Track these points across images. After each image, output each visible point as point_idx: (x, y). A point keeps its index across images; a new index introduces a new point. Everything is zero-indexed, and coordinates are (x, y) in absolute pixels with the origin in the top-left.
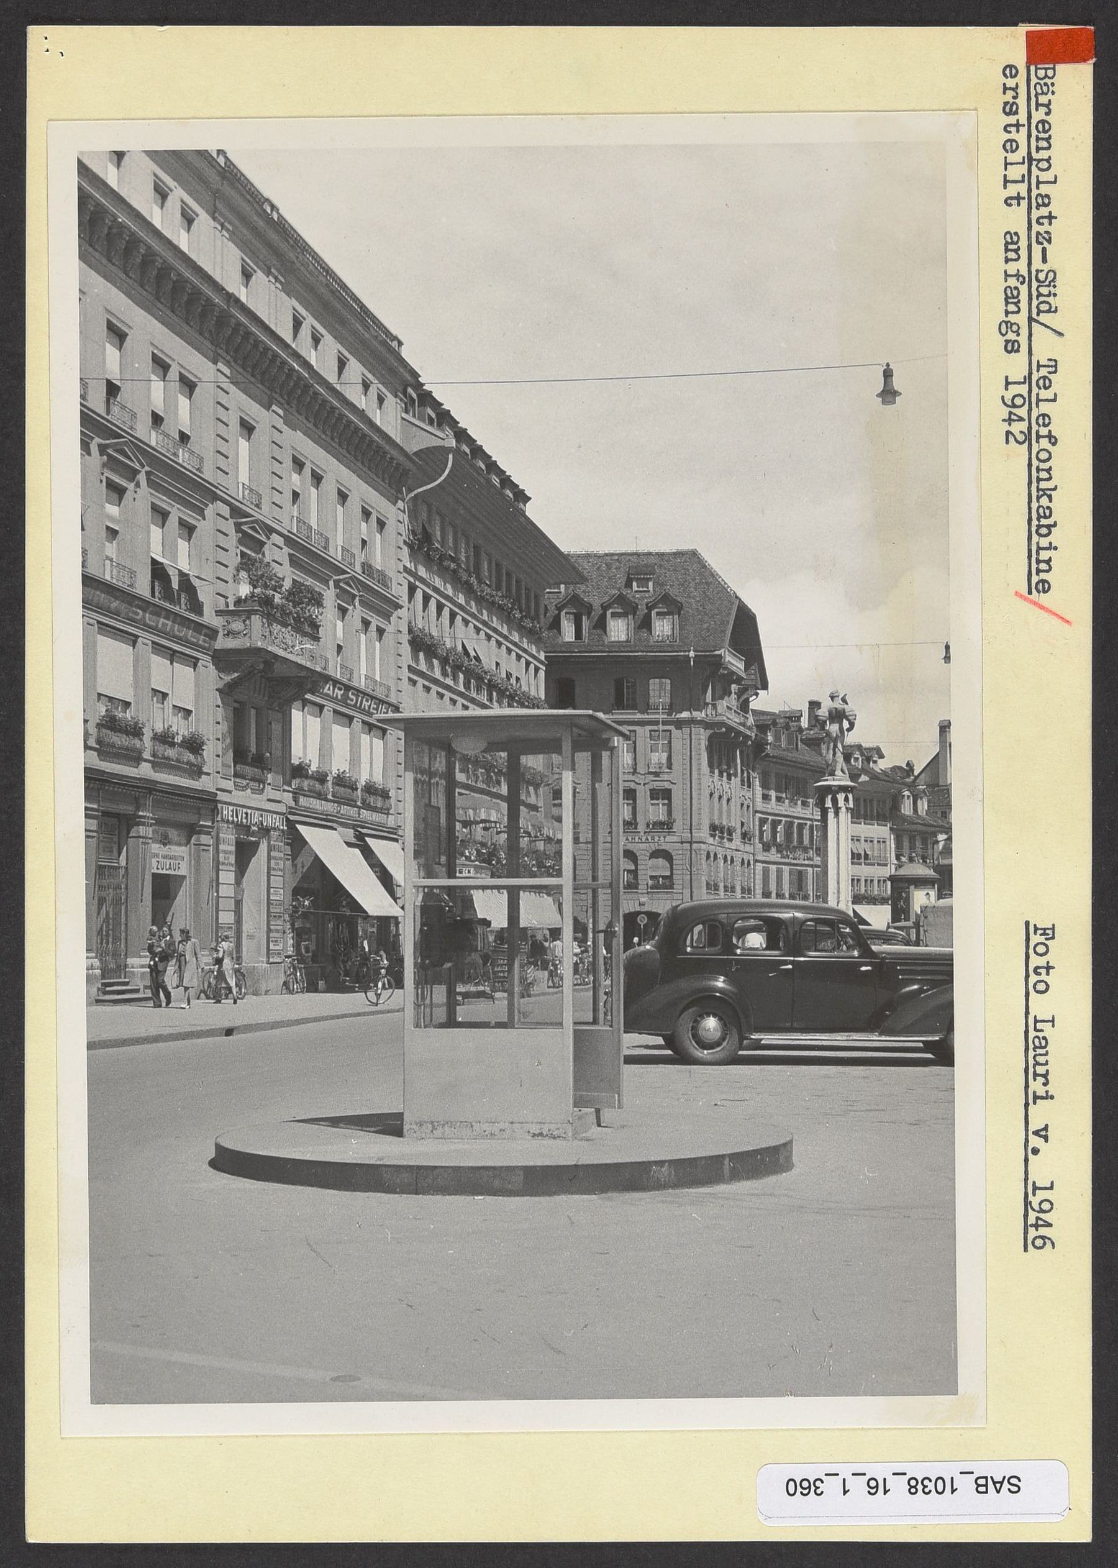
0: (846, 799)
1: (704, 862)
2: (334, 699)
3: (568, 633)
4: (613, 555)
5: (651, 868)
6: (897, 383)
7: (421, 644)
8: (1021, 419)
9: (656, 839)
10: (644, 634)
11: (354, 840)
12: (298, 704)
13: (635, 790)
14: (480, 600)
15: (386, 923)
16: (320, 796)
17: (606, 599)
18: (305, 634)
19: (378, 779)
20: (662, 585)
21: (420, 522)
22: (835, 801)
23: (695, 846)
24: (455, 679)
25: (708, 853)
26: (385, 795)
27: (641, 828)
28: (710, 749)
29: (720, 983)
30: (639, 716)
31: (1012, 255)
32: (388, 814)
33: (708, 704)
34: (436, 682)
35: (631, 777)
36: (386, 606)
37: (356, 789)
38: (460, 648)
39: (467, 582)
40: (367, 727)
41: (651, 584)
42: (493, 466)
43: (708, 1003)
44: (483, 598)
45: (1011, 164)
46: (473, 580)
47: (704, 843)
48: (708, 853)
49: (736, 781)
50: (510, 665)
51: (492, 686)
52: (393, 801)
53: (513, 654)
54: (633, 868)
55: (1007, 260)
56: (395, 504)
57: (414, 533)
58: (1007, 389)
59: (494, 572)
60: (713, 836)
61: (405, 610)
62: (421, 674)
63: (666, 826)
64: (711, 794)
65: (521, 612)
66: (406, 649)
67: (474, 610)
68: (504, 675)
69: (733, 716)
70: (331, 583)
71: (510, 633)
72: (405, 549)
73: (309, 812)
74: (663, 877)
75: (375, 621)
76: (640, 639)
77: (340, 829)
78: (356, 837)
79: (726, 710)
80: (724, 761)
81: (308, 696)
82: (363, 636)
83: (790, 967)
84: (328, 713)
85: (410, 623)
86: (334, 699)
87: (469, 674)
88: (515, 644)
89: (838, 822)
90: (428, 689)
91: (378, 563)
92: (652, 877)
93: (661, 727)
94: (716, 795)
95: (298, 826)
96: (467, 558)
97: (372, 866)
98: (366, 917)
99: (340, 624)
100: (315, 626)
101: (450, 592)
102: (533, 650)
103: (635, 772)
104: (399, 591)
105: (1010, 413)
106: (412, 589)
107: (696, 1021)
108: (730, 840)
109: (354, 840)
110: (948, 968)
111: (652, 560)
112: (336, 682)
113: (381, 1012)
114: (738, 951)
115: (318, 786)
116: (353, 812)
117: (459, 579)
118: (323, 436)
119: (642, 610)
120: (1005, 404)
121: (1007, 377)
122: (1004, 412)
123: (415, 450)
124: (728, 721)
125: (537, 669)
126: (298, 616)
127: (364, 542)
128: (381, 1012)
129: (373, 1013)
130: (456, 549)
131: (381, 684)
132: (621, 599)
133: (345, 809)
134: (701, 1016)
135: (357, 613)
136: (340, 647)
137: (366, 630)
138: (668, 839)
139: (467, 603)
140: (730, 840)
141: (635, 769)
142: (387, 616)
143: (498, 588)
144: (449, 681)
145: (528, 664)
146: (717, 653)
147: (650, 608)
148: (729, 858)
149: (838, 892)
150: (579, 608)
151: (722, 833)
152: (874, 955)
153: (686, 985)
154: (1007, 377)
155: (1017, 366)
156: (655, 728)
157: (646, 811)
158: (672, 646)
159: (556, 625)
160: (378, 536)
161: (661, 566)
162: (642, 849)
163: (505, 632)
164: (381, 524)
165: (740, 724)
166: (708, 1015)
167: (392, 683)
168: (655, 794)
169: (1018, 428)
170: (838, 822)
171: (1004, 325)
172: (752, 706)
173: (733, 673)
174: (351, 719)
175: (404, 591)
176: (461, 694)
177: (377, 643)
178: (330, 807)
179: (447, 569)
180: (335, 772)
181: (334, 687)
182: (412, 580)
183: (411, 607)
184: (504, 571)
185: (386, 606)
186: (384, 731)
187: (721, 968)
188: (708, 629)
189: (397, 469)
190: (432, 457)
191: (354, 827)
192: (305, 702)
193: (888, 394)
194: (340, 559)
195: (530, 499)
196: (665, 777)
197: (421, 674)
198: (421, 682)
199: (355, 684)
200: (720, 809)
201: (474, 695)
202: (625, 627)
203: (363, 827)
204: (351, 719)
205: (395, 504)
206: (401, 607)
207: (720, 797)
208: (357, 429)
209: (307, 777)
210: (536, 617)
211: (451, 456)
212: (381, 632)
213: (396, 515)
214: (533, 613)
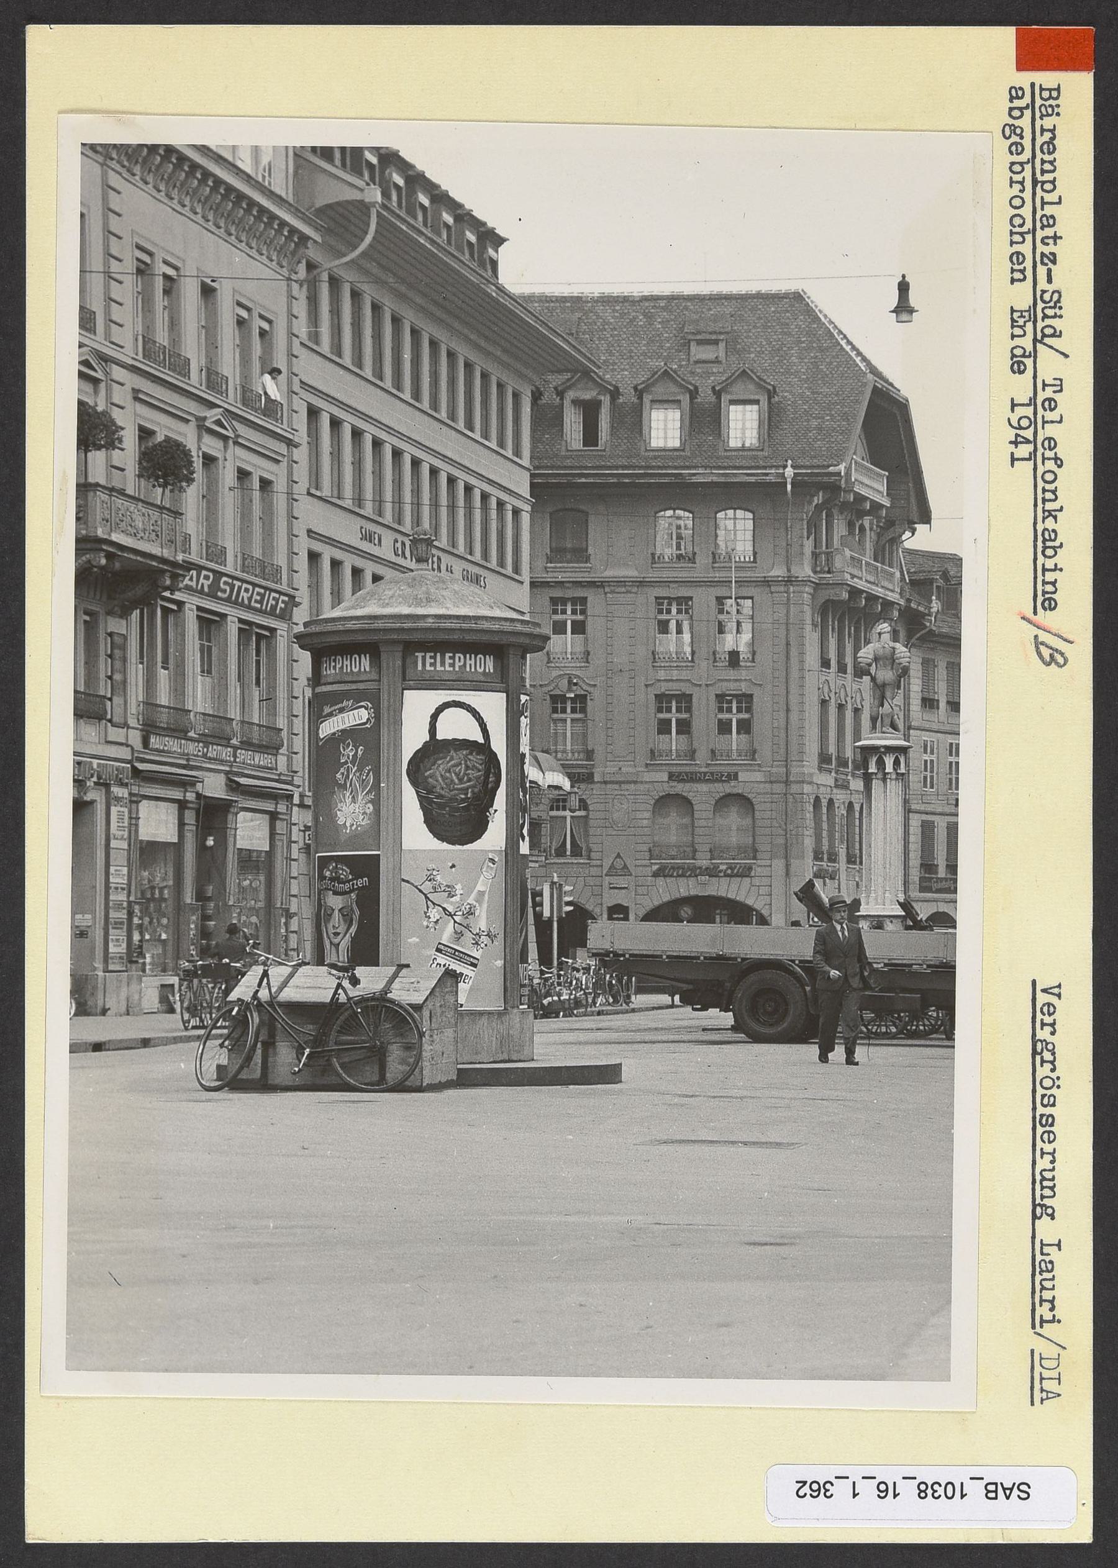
6: (913, 300)
22: (881, 764)
25: (817, 800)
31: (1018, 275)
42: (441, 198)
45: (1018, 459)
48: (817, 800)
55: (1013, 336)
58: (1013, 411)
105: (1017, 435)
116: (226, 753)
120: (1010, 424)
121: (1012, 399)
122: (1011, 434)
154: (1012, 399)
155: (1021, 386)
171: (1007, 128)
193: (903, 308)
207: (841, 707)
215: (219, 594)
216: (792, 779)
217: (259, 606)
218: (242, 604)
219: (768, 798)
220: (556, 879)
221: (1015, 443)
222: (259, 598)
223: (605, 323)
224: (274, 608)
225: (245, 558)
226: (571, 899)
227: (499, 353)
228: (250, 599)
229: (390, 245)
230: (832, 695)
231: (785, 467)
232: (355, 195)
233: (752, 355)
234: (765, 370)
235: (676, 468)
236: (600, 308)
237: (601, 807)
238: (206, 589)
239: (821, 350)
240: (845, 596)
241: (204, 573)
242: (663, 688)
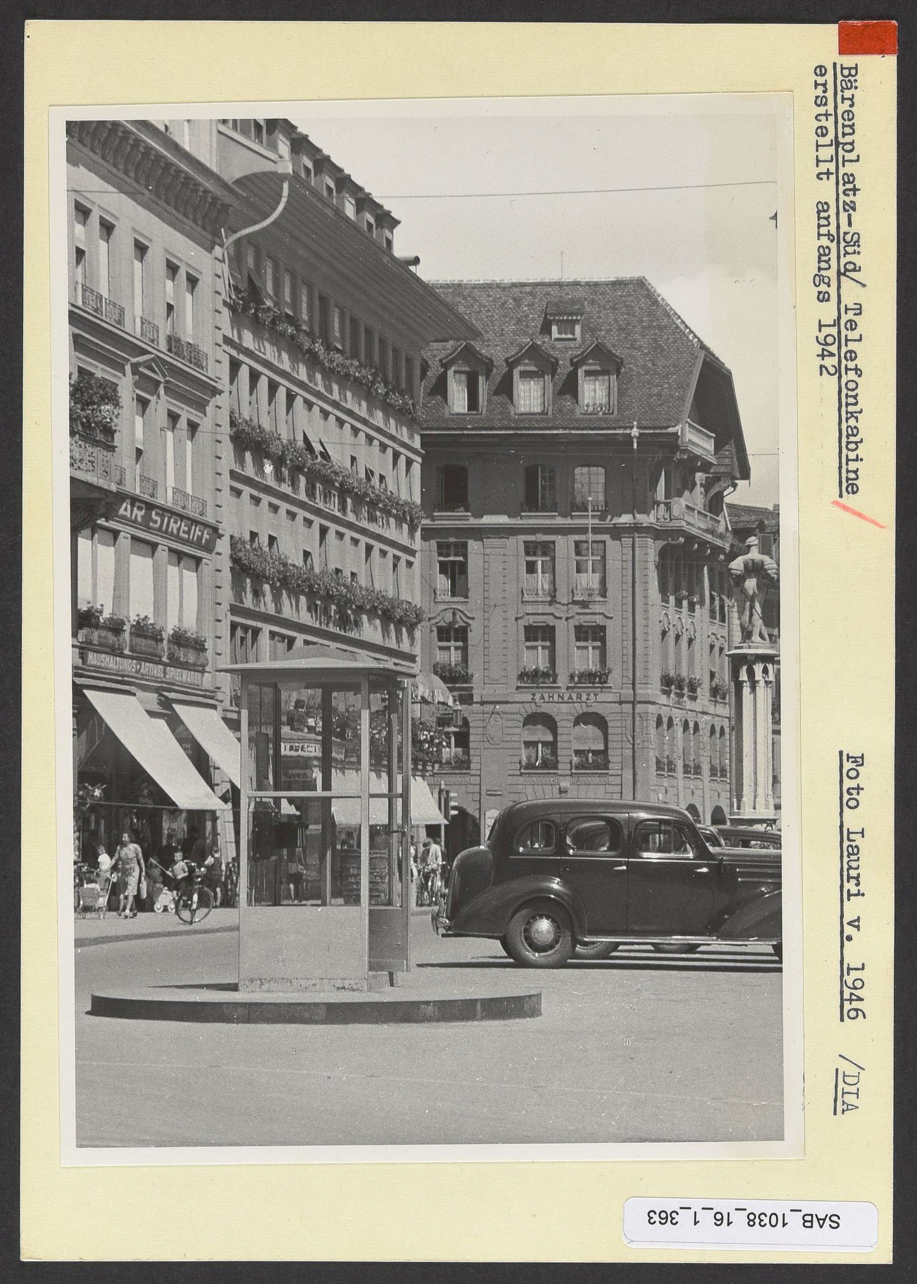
0: (765, 671)
1: (653, 731)
2: (133, 522)
3: (458, 399)
4: (523, 285)
5: (577, 739)
7: (248, 441)
8: (833, 355)
9: (584, 697)
10: (568, 403)
11: (157, 708)
12: (87, 532)
13: (554, 627)
14: (329, 374)
15: (198, 819)
16: (115, 651)
17: (513, 351)
18: (96, 443)
19: (190, 625)
20: (593, 331)
21: (245, 272)
22: (751, 673)
23: (638, 706)
24: (294, 484)
26: (199, 646)
27: (563, 680)
28: (661, 568)
29: (555, 884)
30: (559, 521)
32: (203, 672)
33: (658, 503)
34: (267, 490)
35: (548, 609)
36: (198, 393)
37: (162, 640)
38: (300, 443)
39: (309, 351)
40: (175, 556)
41: (578, 328)
43: (541, 904)
44: (332, 370)
45: (824, 326)
46: (318, 347)
47: (653, 703)
49: (702, 612)
50: (374, 460)
51: (345, 491)
52: (209, 654)
53: (376, 442)
54: (550, 738)
56: (210, 250)
57: (237, 289)
58: (820, 331)
59: (348, 331)
60: (667, 693)
61: (226, 394)
62: (248, 481)
63: (596, 679)
64: (664, 633)
65: (386, 385)
66: (227, 449)
67: (320, 388)
68: (362, 475)
69: (695, 520)
70: (128, 368)
71: (371, 414)
72: (226, 312)
73: (100, 672)
74: (595, 753)
75: (186, 413)
76: (560, 410)
77: (139, 693)
78: (161, 703)
79: (686, 512)
80: (684, 584)
81: (101, 522)
82: (170, 435)
83: (625, 868)
84: (124, 541)
85: (232, 412)
86: (133, 522)
87: (313, 477)
88: (379, 430)
89: (755, 699)
90: (257, 501)
91: (188, 335)
92: (578, 752)
93: (591, 537)
94: (671, 635)
95: (85, 691)
96: (311, 318)
97: (181, 741)
98: (174, 810)
99: (139, 420)
100: (109, 432)
101: (286, 365)
102: (404, 434)
103: (553, 601)
104: (216, 370)
105: (823, 350)
106: (235, 366)
107: (528, 923)
108: (693, 698)
109: (157, 708)
110: (775, 871)
111: (580, 293)
112: (134, 500)
113: (196, 932)
114: (571, 852)
115: (111, 638)
116: (157, 670)
117: (300, 347)
118: (114, 170)
119: (564, 368)
122: (819, 349)
123: (238, 175)
124: (687, 528)
125: (409, 462)
126: (88, 421)
127: (170, 307)
128: (196, 932)
129: (188, 933)
130: (295, 305)
131: (194, 498)
132: (534, 352)
133: (146, 667)
134: (534, 918)
135: (161, 404)
136: (139, 452)
137: (173, 428)
138: (601, 697)
139: (311, 377)
140: (693, 698)
141: (553, 597)
142: (201, 406)
143: (354, 355)
144: (286, 488)
145: (396, 455)
146: (671, 430)
147: (576, 365)
148: (691, 725)
149: (756, 784)
150: (476, 367)
151: (680, 687)
152: (711, 856)
153: (520, 886)
155: (828, 312)
156: (583, 537)
157: (569, 657)
158: (606, 421)
159: (440, 389)
160: (188, 296)
161: (593, 302)
162: (563, 712)
163: (364, 414)
164: (193, 281)
165: (707, 531)
166: (541, 916)
167: (208, 497)
168: (582, 633)
169: (830, 362)
170: (755, 699)
172: (727, 500)
173: (697, 457)
174: (154, 546)
175: (224, 370)
176: (302, 505)
177: (189, 443)
178: (128, 666)
179: (282, 334)
180: (133, 618)
181: (133, 505)
182: (234, 353)
183: (234, 392)
184: (362, 330)
185: (198, 393)
186: (198, 560)
187: (554, 869)
188: (659, 395)
189: (213, 204)
190: (260, 186)
191: (158, 690)
192: (95, 529)
194: (138, 336)
195: (396, 222)
196: (597, 608)
197: (248, 481)
198: (247, 491)
199: (160, 501)
200: (678, 654)
201: (321, 505)
202: (540, 393)
203: (170, 690)
204: (154, 546)
205: (210, 250)
206: (220, 392)
207: (678, 637)
208: (159, 157)
209: (97, 626)
210: (410, 390)
211: (286, 186)
212: (193, 427)
213: (211, 266)
214: (403, 386)
215: (151, 524)
216: (638, 706)
217: (186, 536)
218: (172, 534)
219: (618, 717)
220: (443, 787)
221: (823, 356)
222: (186, 529)
223: (481, 306)
224: (200, 538)
225: (176, 490)
226: (456, 804)
227: (394, 321)
228: (179, 530)
229: (307, 256)
230: (671, 627)
231: (632, 428)
232: (268, 167)
233: (603, 333)
234: (614, 346)
235: (541, 429)
236: (477, 293)
237: (481, 724)
238: (139, 519)
239: (661, 328)
240: (682, 540)
241: (137, 504)
242: (531, 620)
